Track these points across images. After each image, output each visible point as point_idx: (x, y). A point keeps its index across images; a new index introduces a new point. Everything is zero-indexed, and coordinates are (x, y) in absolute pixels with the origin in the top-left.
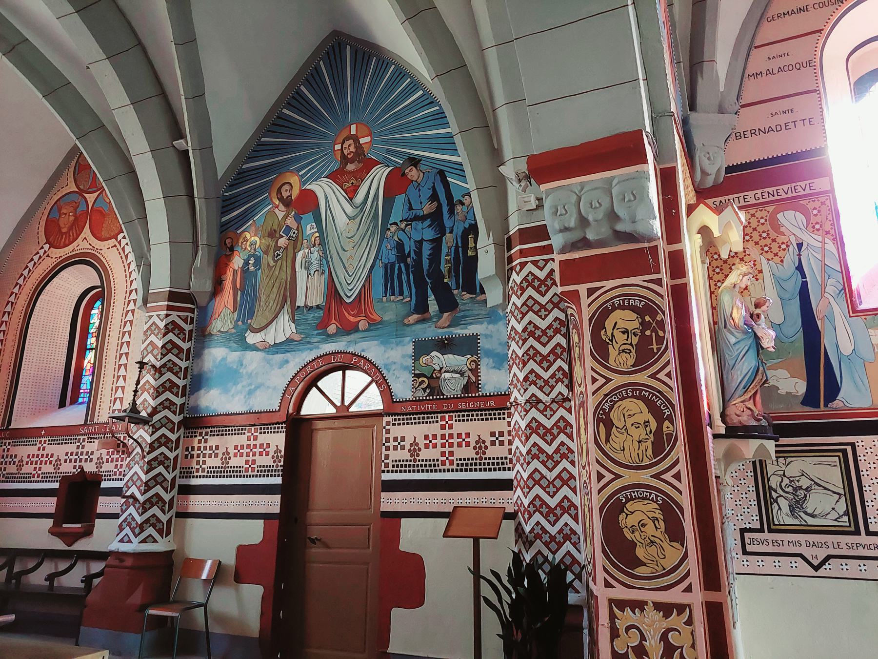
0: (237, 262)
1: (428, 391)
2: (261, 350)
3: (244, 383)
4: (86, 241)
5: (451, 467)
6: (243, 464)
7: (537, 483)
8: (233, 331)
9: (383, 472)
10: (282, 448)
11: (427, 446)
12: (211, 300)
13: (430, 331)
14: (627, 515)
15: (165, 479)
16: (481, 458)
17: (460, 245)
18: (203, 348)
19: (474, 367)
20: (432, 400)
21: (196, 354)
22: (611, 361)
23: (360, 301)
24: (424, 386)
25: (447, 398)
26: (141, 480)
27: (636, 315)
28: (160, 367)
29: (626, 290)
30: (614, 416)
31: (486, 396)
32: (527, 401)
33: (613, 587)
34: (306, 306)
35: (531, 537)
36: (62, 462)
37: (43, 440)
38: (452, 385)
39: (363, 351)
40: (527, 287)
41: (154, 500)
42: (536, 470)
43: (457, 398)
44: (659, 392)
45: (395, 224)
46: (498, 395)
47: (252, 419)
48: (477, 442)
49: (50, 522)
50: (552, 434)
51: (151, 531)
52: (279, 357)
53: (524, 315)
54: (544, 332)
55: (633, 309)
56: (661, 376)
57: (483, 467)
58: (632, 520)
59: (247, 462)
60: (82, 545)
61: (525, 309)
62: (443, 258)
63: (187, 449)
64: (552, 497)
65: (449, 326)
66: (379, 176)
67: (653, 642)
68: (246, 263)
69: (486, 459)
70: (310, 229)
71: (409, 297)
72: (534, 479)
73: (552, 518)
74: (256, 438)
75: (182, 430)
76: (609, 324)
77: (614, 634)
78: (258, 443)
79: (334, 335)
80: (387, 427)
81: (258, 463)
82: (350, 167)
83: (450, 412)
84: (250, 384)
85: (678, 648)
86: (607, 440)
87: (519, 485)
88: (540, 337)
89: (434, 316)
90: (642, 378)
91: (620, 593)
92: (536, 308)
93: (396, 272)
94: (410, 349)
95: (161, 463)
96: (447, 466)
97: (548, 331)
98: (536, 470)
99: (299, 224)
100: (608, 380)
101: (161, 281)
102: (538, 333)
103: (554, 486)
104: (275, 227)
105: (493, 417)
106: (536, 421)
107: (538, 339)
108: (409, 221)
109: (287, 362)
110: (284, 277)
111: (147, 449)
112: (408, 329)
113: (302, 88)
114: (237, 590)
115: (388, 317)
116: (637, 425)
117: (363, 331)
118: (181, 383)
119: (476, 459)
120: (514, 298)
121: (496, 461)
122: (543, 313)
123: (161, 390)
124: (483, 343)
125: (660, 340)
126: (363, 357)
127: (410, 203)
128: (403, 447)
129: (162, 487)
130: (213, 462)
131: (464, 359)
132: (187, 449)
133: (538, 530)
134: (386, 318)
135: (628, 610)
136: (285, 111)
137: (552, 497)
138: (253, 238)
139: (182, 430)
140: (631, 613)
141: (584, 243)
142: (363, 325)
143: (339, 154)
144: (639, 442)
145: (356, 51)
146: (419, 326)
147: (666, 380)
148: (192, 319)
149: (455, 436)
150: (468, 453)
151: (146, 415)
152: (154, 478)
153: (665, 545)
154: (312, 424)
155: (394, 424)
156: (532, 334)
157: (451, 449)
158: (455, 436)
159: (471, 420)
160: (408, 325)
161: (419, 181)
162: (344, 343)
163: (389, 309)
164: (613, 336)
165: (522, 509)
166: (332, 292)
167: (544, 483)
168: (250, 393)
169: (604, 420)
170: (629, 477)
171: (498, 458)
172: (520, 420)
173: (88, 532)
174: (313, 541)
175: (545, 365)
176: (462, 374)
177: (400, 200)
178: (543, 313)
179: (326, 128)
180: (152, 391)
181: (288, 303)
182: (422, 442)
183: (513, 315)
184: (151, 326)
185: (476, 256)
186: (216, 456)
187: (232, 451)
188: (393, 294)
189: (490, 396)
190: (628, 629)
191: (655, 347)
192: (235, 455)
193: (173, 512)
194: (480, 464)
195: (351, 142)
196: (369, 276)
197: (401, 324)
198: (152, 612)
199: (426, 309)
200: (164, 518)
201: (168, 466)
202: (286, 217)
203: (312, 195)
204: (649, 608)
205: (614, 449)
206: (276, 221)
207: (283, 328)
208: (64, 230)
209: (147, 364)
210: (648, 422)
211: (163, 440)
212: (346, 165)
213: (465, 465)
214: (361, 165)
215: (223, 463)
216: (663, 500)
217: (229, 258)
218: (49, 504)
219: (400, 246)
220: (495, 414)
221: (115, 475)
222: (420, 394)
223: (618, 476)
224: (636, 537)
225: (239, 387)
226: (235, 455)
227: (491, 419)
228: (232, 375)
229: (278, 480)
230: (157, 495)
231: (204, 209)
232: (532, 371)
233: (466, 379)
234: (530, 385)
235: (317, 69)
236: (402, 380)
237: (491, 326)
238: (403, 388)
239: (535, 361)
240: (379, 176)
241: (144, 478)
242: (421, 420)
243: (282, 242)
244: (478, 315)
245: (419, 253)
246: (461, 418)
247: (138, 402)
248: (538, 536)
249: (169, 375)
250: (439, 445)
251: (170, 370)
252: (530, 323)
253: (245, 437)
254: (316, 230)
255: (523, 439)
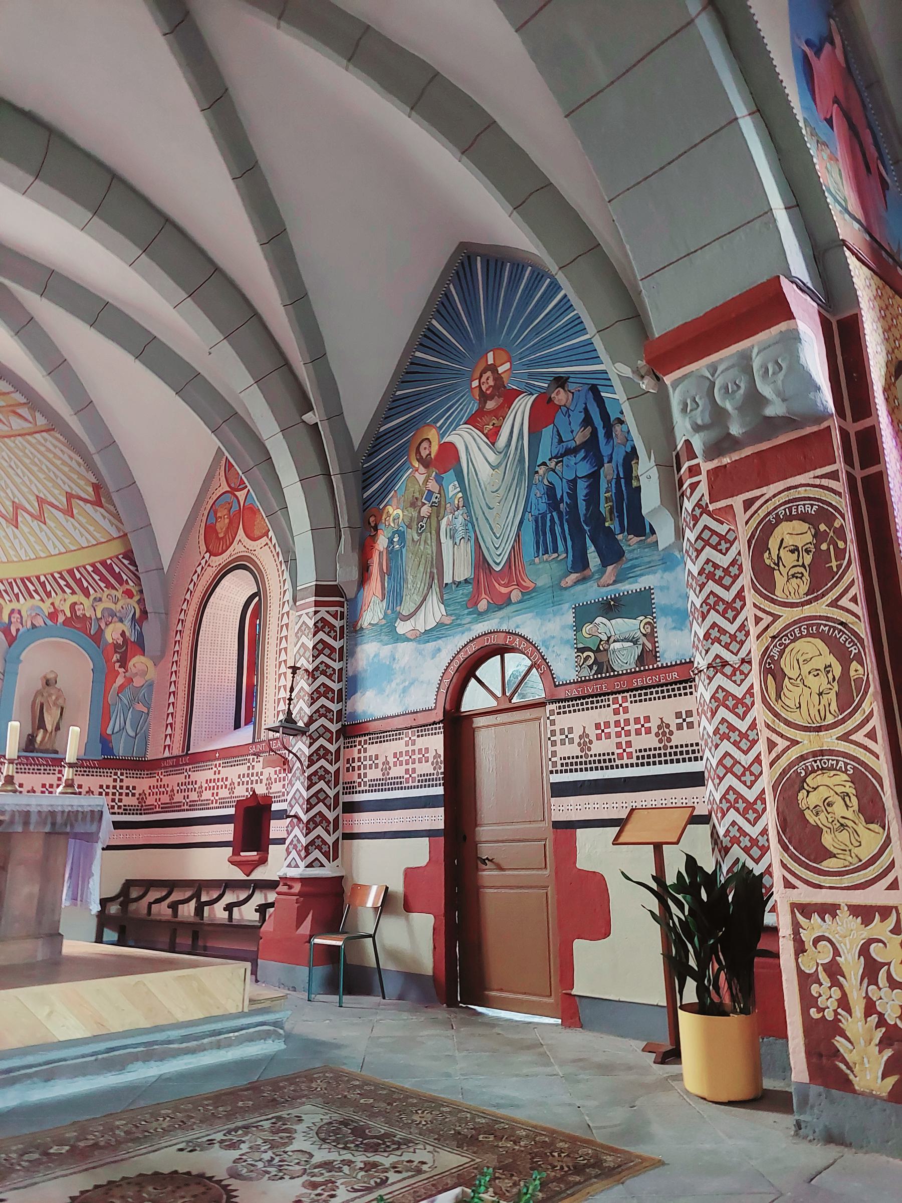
0: (382, 542)
1: (595, 668)
2: (411, 640)
3: (398, 681)
4: (241, 545)
5: (629, 762)
6: (402, 774)
7: (729, 770)
8: (384, 622)
9: (551, 772)
10: (441, 752)
11: (599, 738)
12: (358, 590)
13: (593, 592)
14: (808, 792)
15: (328, 796)
16: (665, 747)
17: (622, 476)
18: (356, 645)
19: (649, 630)
20: (601, 681)
21: (344, 654)
22: (778, 592)
23: (510, 567)
24: (591, 662)
25: (619, 675)
26: (303, 798)
27: (807, 525)
28: (313, 671)
29: (793, 494)
30: (786, 664)
31: (667, 666)
32: (709, 666)
33: (794, 887)
34: (454, 582)
35: (726, 841)
36: (236, 785)
37: (218, 763)
38: (624, 657)
39: (518, 627)
40: (701, 515)
41: (318, 819)
42: (727, 754)
43: (631, 673)
44: (842, 623)
45: (544, 464)
46: (681, 663)
47: (408, 721)
48: (659, 727)
49: (229, 851)
50: (744, 705)
51: (317, 854)
52: (431, 646)
53: (699, 552)
54: (726, 571)
55: (803, 517)
56: (844, 602)
57: (668, 758)
58: (814, 799)
59: (407, 771)
60: (259, 874)
61: (700, 544)
62: (603, 495)
63: (348, 762)
64: (750, 788)
65: (615, 582)
66: (523, 406)
67: (849, 957)
68: (391, 541)
69: (671, 747)
70: (452, 490)
71: (565, 552)
72: (725, 767)
73: (751, 816)
74: (414, 743)
75: (342, 739)
76: (773, 544)
77: (800, 948)
78: (416, 748)
79: (486, 612)
80: (551, 718)
81: (418, 772)
82: (490, 405)
83: (623, 692)
84: (404, 681)
85: (884, 964)
86: (778, 697)
87: (709, 776)
88: (721, 578)
89: (597, 572)
90: (820, 608)
91: (805, 895)
92: (715, 540)
93: (548, 524)
94: (570, 618)
95: (322, 778)
96: (625, 761)
97: (731, 569)
98: (727, 754)
99: (441, 486)
100: (776, 617)
101: (308, 578)
102: (719, 573)
103: (752, 774)
104: (417, 495)
105: (677, 692)
106: (723, 690)
107: (719, 582)
108: (559, 457)
109: (439, 650)
110: (430, 552)
111: (306, 763)
112: (566, 593)
113: (434, 322)
114: (407, 919)
115: (543, 581)
116: (816, 673)
117: (515, 603)
118: (335, 686)
119: (660, 749)
120: (688, 532)
121: (684, 749)
122: (724, 546)
123: (315, 696)
124: (658, 599)
125: (840, 554)
126: (518, 635)
127: (559, 435)
128: (133, 795)
129: (325, 804)
130: (374, 774)
131: (636, 622)
132: (348, 762)
133: (734, 832)
134: (540, 584)
135: (816, 917)
136: (418, 354)
137: (750, 788)
138: (395, 512)
139: (342, 739)
140: (819, 920)
141: (734, 443)
142: (516, 595)
143: (477, 392)
144: (820, 694)
145: (488, 261)
146: (580, 588)
147: (852, 606)
148: (342, 613)
149: (632, 721)
150: (650, 741)
151: (303, 725)
152: (316, 795)
153: (861, 828)
154: (472, 722)
155: (559, 713)
156: (711, 576)
157: (628, 739)
158: (632, 721)
159: (650, 699)
160: (566, 588)
161: (567, 405)
162: (497, 621)
163: (543, 571)
164: (779, 558)
165: (715, 806)
166: (481, 563)
167: (738, 770)
168: (405, 690)
169: (773, 670)
170: (809, 743)
171: (687, 746)
172: (704, 691)
173: (263, 861)
174: (484, 862)
175: (730, 614)
176: (635, 642)
177: (547, 433)
178: (724, 546)
179: (460, 363)
180: (306, 698)
181: (436, 581)
182: (592, 733)
183: (688, 555)
184: (301, 626)
185: (640, 487)
186: (377, 766)
187: (391, 760)
188: (546, 552)
189: (672, 666)
190: (816, 941)
191: (834, 564)
192: (395, 764)
193: (339, 833)
194: (665, 755)
195: (489, 373)
196: (518, 535)
197: (558, 588)
198: (317, 941)
199: (585, 565)
200: (330, 840)
201: (330, 781)
202: (426, 481)
203: (452, 445)
204: (843, 913)
205: (785, 707)
206: (417, 486)
207: (434, 612)
208: (221, 535)
209: (299, 668)
210: (830, 666)
211: (322, 752)
212: (486, 403)
213: (646, 757)
214: (501, 400)
215: (383, 775)
216: (854, 768)
217: (374, 538)
218: (226, 832)
219: (551, 490)
220: (679, 689)
221: (407, 782)
222: (586, 673)
223: (794, 743)
224: (821, 820)
225: (393, 685)
226: (395, 764)
227: (675, 696)
228: (386, 671)
229: (440, 791)
230: (320, 813)
231: (341, 486)
232: (714, 625)
233: (641, 647)
234: (712, 644)
235: (447, 295)
236: (563, 657)
237: (668, 576)
238: (566, 667)
239: (717, 611)
240: (523, 406)
241: (305, 795)
242: (643, 698)
243: (425, 510)
244: (650, 562)
245: (573, 496)
246: (638, 698)
247: (294, 713)
248: (735, 841)
249: (323, 679)
250: (613, 735)
251: (324, 673)
252: (708, 561)
253: (402, 742)
254: (459, 489)
255: (709, 714)
